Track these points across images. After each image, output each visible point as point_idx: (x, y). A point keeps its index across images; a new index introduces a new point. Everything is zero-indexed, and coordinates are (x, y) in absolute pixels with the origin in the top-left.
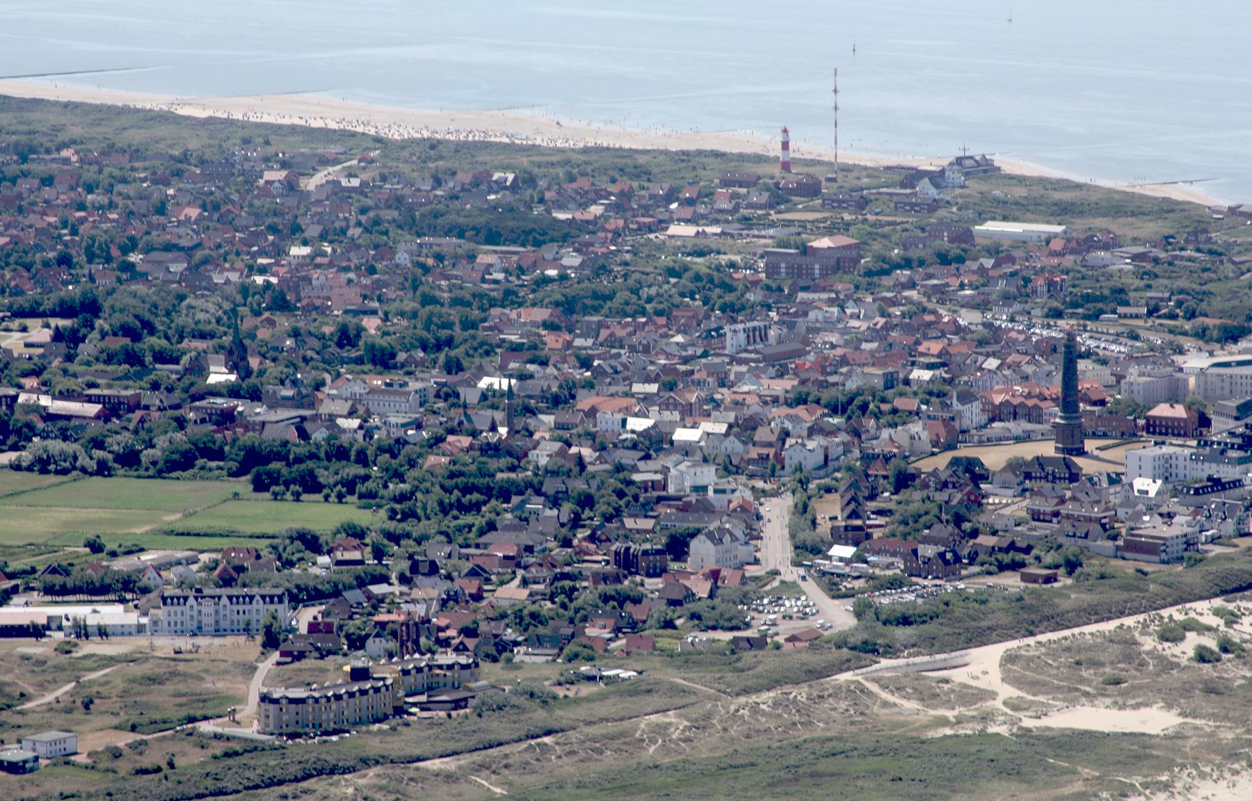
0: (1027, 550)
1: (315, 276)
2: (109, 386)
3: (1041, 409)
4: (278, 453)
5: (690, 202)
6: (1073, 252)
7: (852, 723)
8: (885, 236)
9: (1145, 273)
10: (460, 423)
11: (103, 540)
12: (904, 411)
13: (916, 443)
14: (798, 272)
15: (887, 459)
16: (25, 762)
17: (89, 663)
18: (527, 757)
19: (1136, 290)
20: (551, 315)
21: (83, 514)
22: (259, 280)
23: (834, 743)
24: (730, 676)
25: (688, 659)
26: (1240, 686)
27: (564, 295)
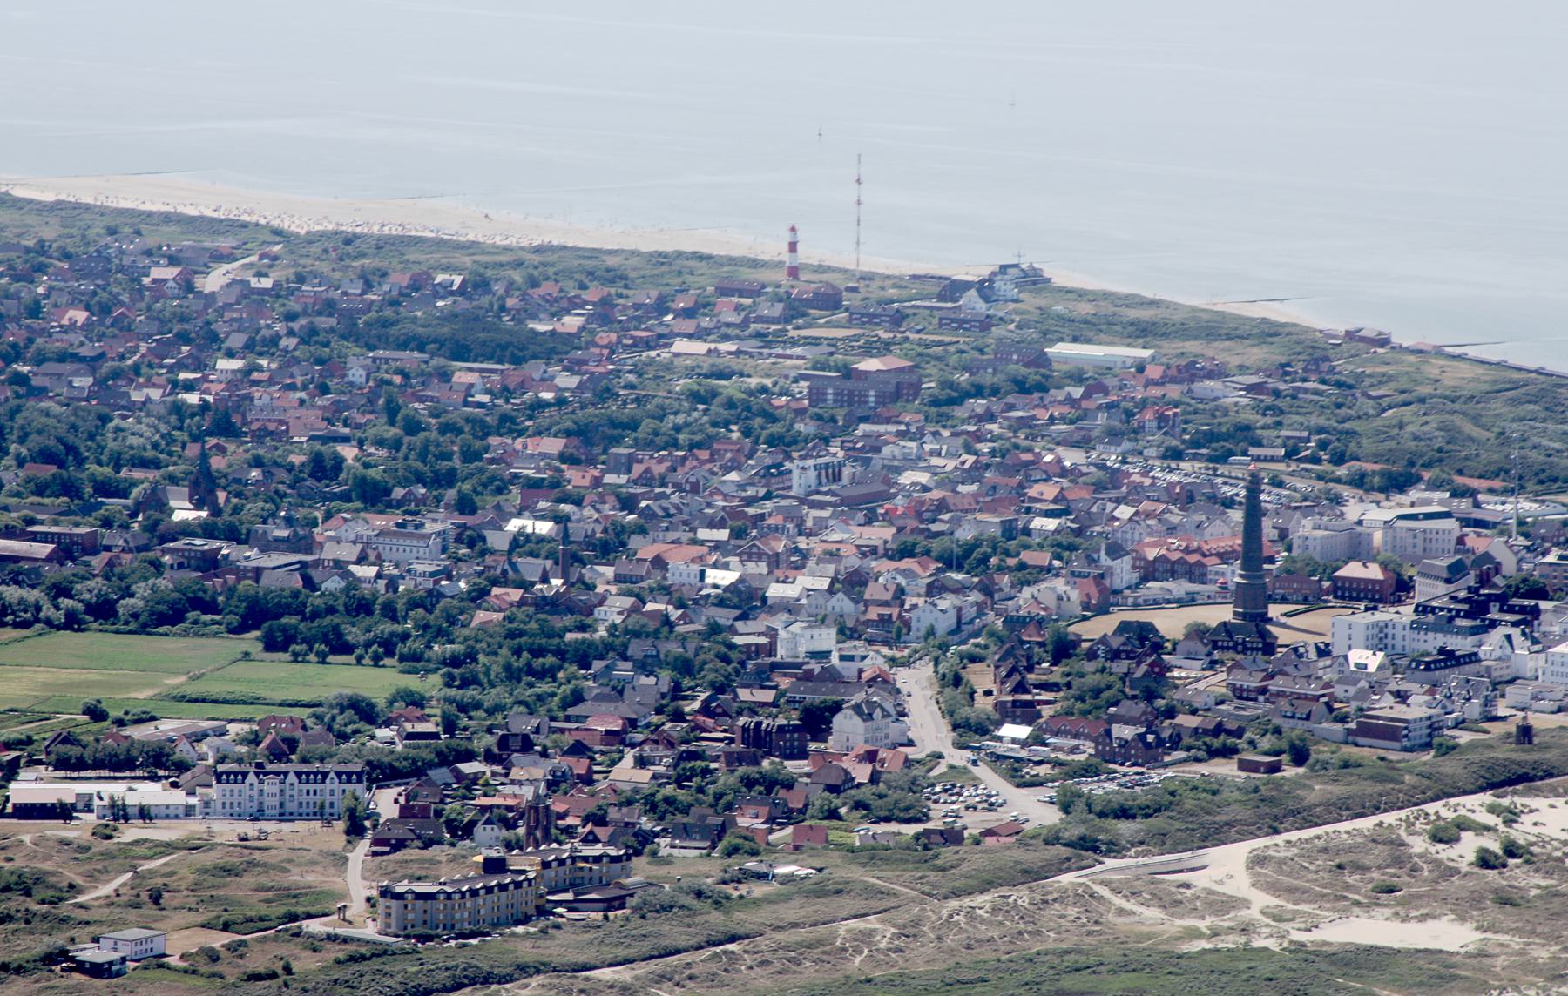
0: (1239, 733)
1: (257, 395)
2: (56, 523)
3: (1204, 566)
4: (288, 606)
5: (689, 313)
6: (1173, 380)
7: (1089, 933)
8: (937, 358)
9: (1268, 408)
10: (504, 572)
11: (104, 706)
12: (1035, 567)
13: (1064, 604)
14: (846, 403)
15: (1040, 623)
16: (111, 963)
17: (142, 850)
18: (713, 966)
19: (1263, 428)
20: (566, 446)
21: (64, 675)
22: (193, 399)
23: (1073, 957)
24: (933, 876)
25: (872, 854)
26: (1537, 897)
27: (575, 423)
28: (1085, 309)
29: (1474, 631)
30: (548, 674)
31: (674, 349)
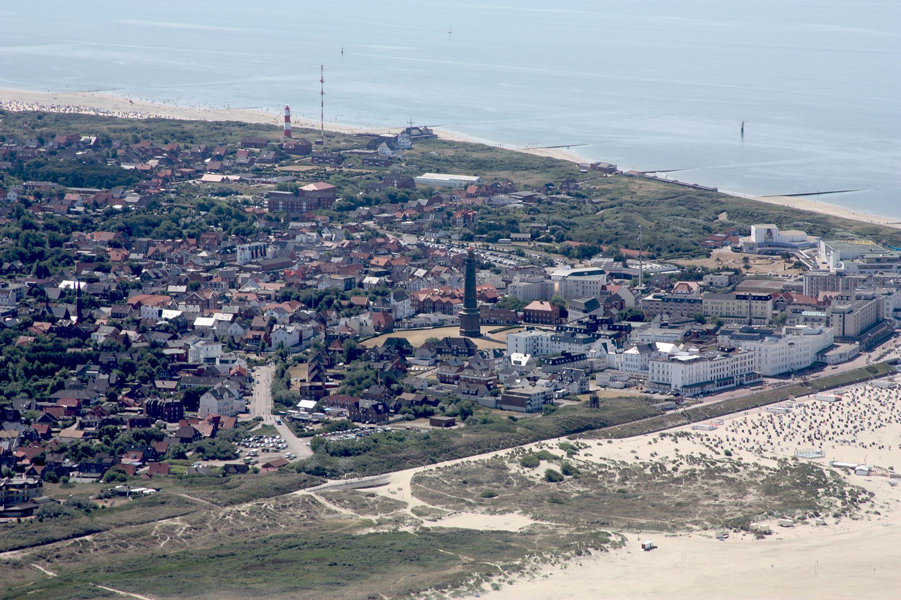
5: (219, 158)
8: (354, 183)
9: (531, 210)
10: (44, 313)
13: (364, 328)
14: (292, 207)
18: (73, 550)
20: (115, 237)
24: (220, 492)
26: (576, 498)
28: (450, 153)
29: (585, 341)
30: (51, 373)
31: (203, 179)
